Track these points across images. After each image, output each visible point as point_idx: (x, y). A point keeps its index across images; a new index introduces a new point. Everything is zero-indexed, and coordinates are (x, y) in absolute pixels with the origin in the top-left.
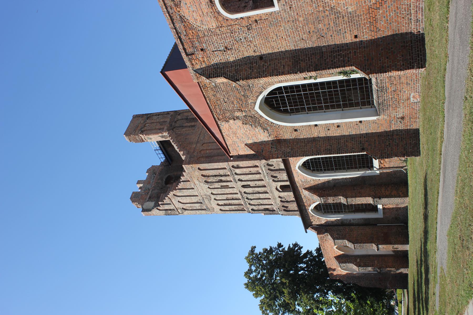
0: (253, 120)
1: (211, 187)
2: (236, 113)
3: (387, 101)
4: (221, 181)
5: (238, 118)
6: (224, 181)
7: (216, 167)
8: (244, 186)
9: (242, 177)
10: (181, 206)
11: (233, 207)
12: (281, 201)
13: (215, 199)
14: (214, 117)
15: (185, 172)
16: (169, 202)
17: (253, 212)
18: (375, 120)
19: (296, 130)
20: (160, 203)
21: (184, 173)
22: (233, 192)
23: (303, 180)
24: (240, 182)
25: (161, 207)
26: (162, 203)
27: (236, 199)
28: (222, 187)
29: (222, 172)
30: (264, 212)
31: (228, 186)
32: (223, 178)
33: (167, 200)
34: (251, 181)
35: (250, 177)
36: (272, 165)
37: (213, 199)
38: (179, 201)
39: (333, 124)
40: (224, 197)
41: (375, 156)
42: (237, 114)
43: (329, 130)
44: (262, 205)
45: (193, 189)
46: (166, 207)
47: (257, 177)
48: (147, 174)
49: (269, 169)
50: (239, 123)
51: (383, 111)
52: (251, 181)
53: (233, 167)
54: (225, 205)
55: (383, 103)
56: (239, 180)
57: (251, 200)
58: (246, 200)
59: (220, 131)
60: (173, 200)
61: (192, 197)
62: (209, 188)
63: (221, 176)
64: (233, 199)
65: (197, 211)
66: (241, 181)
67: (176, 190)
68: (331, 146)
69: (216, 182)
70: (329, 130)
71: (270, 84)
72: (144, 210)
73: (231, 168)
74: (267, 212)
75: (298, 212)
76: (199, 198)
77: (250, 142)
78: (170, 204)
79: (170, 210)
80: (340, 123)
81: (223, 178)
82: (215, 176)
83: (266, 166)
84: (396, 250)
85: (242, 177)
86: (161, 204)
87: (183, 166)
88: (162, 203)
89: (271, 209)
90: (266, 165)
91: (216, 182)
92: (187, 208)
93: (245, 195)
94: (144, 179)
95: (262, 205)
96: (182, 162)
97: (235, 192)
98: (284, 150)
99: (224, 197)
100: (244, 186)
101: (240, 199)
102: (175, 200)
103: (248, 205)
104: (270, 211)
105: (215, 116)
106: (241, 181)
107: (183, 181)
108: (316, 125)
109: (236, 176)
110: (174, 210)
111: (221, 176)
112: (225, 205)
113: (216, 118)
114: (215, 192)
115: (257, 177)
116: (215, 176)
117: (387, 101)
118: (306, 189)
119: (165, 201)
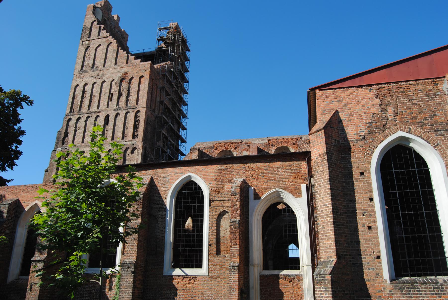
0: (378, 126)
1: (113, 83)
2: (393, 109)
3: (417, 294)
4: (120, 95)
5: (384, 110)
6: (119, 98)
7: (141, 94)
8: (107, 117)
9: (121, 119)
10: (93, 45)
11: (78, 99)
12: (127, 149)
13: (95, 83)
14: (385, 83)
15: (141, 62)
16: (101, 35)
17: (67, 120)
18: (382, 277)
19: (362, 174)
20: (102, 26)
21: (140, 60)
22: (101, 103)
23: (167, 179)
24: (114, 113)
25: (96, 26)
26: (102, 28)
27: (90, 105)
28: (111, 96)
29: (133, 99)
30: (64, 131)
31: (111, 101)
32: (123, 98)
33: (104, 33)
34: (114, 126)
35: (120, 126)
36: (132, 152)
37: (95, 80)
38: (100, 45)
39: (375, 222)
40: (96, 93)
41: (334, 273)
42: (390, 111)
43: (364, 215)
44: (76, 131)
45: (116, 64)
46: (95, 31)
47: (119, 134)
48: (123, 30)
49: (127, 149)
50: (376, 110)
51: (400, 289)
52: (114, 126)
53: (138, 111)
54: (84, 92)
55: (415, 288)
56: (118, 114)
57: (86, 121)
58: (87, 116)
59: (361, 86)
60: (103, 40)
61: (103, 60)
62: (114, 80)
63: (128, 97)
64: (90, 102)
65: (82, 60)
66: (116, 116)
67: (118, 46)
68: (340, 215)
69: (120, 90)
70: (364, 215)
71: (182, 174)
72: (95, 7)
73: (137, 110)
74: (63, 135)
75: (121, 164)
76: (101, 67)
77: (342, 116)
78: (99, 35)
79: (90, 34)
80: (377, 230)
81: (123, 98)
82: (129, 91)
83: (133, 146)
84: (29, 287)
85: (121, 119)
86: (100, 27)
87: (150, 62)
88: (102, 28)
89: (65, 140)
90: (135, 146)
91: (120, 90)
92: (88, 52)
93: (94, 116)
94: (121, 25)
95: (76, 131)
96: (153, 63)
97: (101, 107)
98: (333, 154)
99: (96, 93)
100: (107, 117)
101: (89, 110)
102: (103, 42)
103: (79, 116)
104: (64, 138)
105: (386, 85)
106: (116, 116)
107: (128, 57)
108: (371, 200)
109: (124, 112)
110: (89, 37)
111: (128, 97)
112: (84, 92)
113: (383, 86)
114: (106, 86)
115: (119, 134)
116: (129, 91)
117: (417, 294)
118: (152, 179)
119: (105, 31)
